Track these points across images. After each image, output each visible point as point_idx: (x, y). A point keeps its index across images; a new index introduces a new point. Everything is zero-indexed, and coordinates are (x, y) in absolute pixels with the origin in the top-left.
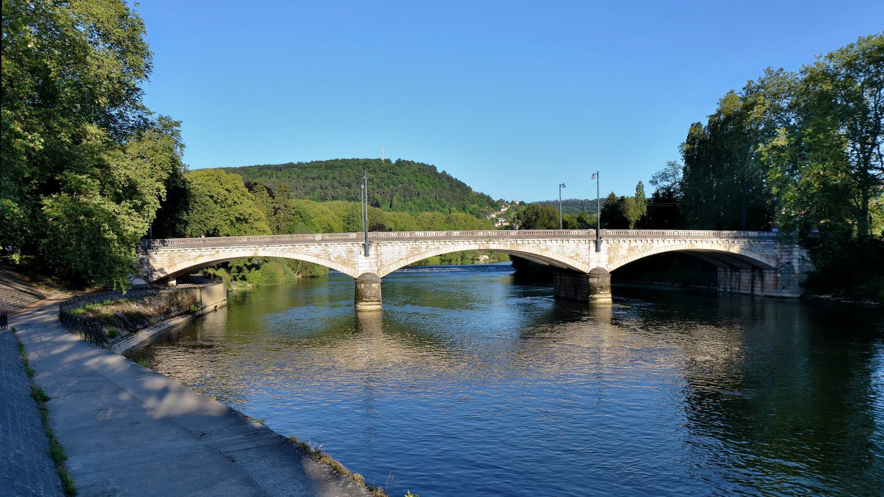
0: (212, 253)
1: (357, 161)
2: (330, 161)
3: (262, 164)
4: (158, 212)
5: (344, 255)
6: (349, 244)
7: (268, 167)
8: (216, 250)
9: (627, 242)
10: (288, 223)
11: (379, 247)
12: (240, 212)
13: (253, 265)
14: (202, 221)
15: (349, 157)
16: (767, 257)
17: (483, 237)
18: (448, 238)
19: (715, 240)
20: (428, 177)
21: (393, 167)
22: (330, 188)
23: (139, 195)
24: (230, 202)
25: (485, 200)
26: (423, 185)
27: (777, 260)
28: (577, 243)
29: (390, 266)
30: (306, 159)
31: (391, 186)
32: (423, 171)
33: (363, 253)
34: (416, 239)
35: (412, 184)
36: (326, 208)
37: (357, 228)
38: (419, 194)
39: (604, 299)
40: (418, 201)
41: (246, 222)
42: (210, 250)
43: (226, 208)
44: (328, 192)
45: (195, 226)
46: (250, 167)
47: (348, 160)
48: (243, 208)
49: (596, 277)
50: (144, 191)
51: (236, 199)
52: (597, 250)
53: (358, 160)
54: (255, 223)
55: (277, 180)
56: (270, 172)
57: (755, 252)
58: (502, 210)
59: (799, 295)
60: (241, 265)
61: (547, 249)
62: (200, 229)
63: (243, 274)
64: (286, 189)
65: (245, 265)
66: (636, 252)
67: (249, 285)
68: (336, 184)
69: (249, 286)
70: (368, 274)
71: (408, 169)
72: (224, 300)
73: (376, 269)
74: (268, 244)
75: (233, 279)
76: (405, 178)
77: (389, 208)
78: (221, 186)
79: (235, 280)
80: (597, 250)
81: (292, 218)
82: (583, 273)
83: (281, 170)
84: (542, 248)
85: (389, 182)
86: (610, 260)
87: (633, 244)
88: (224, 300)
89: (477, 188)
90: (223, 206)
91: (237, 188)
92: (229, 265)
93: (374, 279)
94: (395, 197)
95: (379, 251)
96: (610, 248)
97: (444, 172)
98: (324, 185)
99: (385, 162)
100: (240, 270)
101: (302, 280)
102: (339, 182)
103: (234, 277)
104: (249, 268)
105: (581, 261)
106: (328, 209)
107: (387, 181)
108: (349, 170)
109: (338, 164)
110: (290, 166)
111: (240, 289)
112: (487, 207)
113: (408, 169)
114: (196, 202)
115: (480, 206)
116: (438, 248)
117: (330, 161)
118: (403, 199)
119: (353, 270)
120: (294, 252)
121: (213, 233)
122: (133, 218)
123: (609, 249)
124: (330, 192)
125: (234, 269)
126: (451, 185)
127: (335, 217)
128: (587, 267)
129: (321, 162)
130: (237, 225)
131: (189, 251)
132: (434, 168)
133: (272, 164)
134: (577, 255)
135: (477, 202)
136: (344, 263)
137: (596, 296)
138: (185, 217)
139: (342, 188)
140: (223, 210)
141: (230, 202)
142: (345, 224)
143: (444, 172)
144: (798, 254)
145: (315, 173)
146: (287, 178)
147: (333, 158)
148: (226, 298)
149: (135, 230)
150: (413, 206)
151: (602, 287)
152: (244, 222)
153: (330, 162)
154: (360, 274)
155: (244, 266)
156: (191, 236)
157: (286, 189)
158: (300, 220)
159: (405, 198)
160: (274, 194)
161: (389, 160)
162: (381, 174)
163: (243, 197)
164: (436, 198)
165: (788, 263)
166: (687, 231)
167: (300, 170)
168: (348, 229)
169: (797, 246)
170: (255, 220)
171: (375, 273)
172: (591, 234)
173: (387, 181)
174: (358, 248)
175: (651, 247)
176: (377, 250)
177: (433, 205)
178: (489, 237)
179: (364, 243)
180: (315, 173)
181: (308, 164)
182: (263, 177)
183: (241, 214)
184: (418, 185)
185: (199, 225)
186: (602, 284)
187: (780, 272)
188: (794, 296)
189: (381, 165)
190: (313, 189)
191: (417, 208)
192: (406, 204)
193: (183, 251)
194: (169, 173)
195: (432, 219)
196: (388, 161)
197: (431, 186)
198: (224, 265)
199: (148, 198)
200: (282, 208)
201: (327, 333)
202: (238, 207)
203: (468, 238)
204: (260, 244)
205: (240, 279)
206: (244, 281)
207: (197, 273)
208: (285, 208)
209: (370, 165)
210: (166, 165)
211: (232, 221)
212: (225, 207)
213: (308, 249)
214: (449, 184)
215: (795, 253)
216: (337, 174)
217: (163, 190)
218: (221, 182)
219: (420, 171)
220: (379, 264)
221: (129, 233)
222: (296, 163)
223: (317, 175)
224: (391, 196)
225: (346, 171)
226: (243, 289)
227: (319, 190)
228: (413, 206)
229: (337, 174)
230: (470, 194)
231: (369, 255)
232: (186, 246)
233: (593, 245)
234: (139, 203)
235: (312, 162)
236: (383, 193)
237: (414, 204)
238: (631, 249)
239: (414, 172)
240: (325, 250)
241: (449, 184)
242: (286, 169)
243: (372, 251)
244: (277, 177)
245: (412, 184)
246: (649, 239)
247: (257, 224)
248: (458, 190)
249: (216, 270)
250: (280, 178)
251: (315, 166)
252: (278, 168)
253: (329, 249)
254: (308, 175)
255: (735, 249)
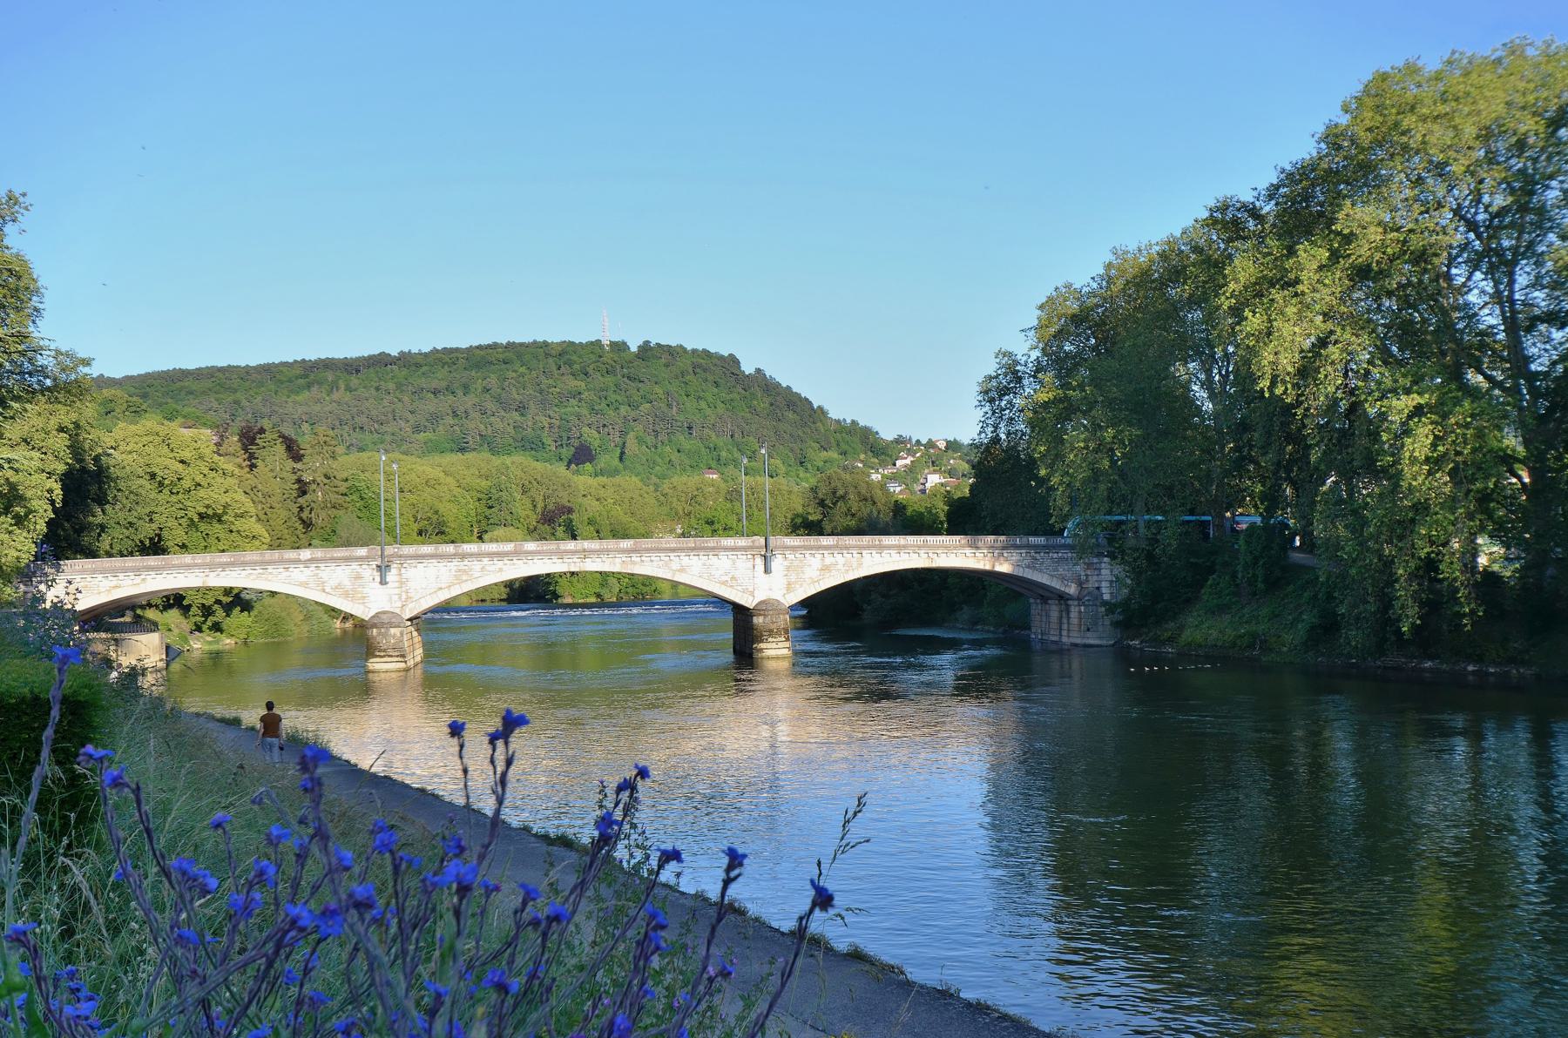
0: (135, 582)
1: (541, 349)
2: (477, 347)
3: (312, 356)
4: (50, 523)
5: (347, 583)
6: (355, 566)
7: (327, 364)
8: (142, 577)
9: (819, 556)
10: (333, 512)
11: (403, 571)
12: (207, 502)
13: (237, 601)
14: (130, 523)
15: (526, 338)
16: (1063, 579)
17: (574, 552)
18: (517, 553)
19: (968, 551)
20: (716, 384)
21: (631, 362)
22: (477, 415)
23: (21, 499)
24: (186, 483)
25: (856, 439)
26: (703, 404)
27: (1080, 584)
28: (733, 561)
29: (422, 601)
30: (421, 342)
31: (624, 410)
32: (705, 370)
33: (378, 579)
34: (463, 556)
35: (675, 404)
36: (436, 473)
37: (509, 518)
38: (690, 428)
39: (776, 650)
40: (687, 444)
41: (220, 521)
42: (133, 577)
43: (180, 496)
44: (472, 425)
45: (119, 533)
46: (282, 364)
47: (521, 345)
48: (212, 494)
49: (761, 615)
50: (29, 494)
51: (199, 478)
52: (767, 570)
53: (545, 344)
54: (236, 522)
55: (348, 397)
56: (330, 376)
57: (1041, 571)
58: (899, 463)
59: (1112, 642)
60: (209, 601)
61: (682, 570)
62: (128, 537)
63: (215, 619)
64: (328, 439)
65: (218, 602)
66: (833, 573)
67: (228, 641)
68: (490, 406)
69: (227, 642)
70: (385, 613)
71: (667, 366)
72: (161, 660)
73: (399, 604)
74: (224, 566)
75: (194, 628)
76: (658, 389)
77: (616, 462)
78: (171, 455)
79: (199, 629)
80: (767, 570)
81: (340, 501)
82: (748, 609)
83: (358, 371)
84: (674, 568)
85: (619, 398)
86: (789, 588)
87: (829, 560)
88: (161, 660)
89: (838, 411)
90: (174, 491)
91: (201, 458)
92: (185, 603)
93: (393, 620)
94: (631, 435)
95: (404, 576)
96: (789, 567)
97: (758, 371)
98: (462, 409)
99: (612, 350)
100: (207, 611)
101: (354, 632)
102: (498, 399)
103: (195, 624)
104: (228, 609)
105: (739, 588)
106: (442, 475)
107: (613, 397)
108: (523, 370)
109: (497, 356)
110: (380, 362)
111: (207, 648)
112: (862, 456)
113: (667, 366)
114: (119, 490)
115: (844, 453)
116: (501, 570)
117: (479, 347)
118: (650, 440)
119: (362, 607)
120: (266, 579)
121: (155, 547)
122: (15, 538)
123: (788, 568)
124: (475, 424)
125: (194, 610)
126: (772, 405)
127: (457, 491)
128: (751, 598)
129: (457, 350)
130: (203, 526)
131: (100, 579)
132: (733, 361)
133: (336, 357)
134: (733, 578)
135: (838, 445)
136: (346, 595)
137: (762, 645)
138: (99, 518)
139: (503, 413)
140: (174, 498)
141: (186, 483)
142: (482, 509)
143: (758, 371)
144: (1108, 572)
145: (440, 378)
146: (373, 391)
147: (486, 340)
148: (164, 657)
149: (18, 554)
150: (675, 457)
151: (771, 631)
152: (215, 521)
153: (478, 352)
154: (372, 613)
155: (215, 603)
156: (109, 555)
157: (328, 439)
158: (358, 505)
159: (656, 437)
160: (302, 452)
161: (624, 343)
162: (599, 380)
163: (213, 474)
164: (732, 436)
165: (1098, 588)
166: (922, 538)
167: (405, 372)
168: (489, 519)
169: (1106, 559)
170: (236, 516)
171: (398, 611)
172: (757, 544)
173: (613, 397)
174: (369, 572)
175: (860, 565)
176: (400, 575)
177: (724, 454)
178: (584, 551)
179: (379, 563)
180: (440, 378)
181: (426, 355)
182: (315, 389)
183: (208, 507)
184: (690, 404)
185: (125, 531)
186: (773, 627)
187: (1084, 604)
188: (1104, 642)
189: (600, 357)
190: (435, 418)
191: (687, 462)
192: (659, 450)
193: (89, 579)
194: (67, 464)
195: (696, 493)
196: (619, 347)
197: (721, 408)
198: (175, 600)
199: (35, 504)
200: (318, 480)
201: (867, 961)
202: (202, 493)
203: (550, 553)
204: (212, 567)
205: (210, 629)
206: (219, 633)
207: (123, 616)
208: (326, 481)
209: (574, 358)
210: (62, 453)
211: (191, 520)
212: (178, 492)
213: (288, 574)
214: (767, 400)
215: (1103, 572)
216: (493, 380)
217: (56, 492)
218: (171, 446)
219: (698, 370)
220: (404, 596)
221: (9, 558)
222: (394, 353)
223: (444, 384)
224: (623, 434)
225: (516, 371)
226: (215, 647)
227: (450, 420)
228: (675, 457)
229: (493, 380)
230: (819, 424)
231: (386, 583)
232: (94, 571)
233: (759, 562)
234: (22, 512)
235: (435, 351)
236: (604, 426)
237: (679, 451)
238: (826, 569)
239: (682, 373)
240: (317, 575)
241: (767, 400)
242: (371, 370)
243: (391, 576)
244: (348, 389)
245: (675, 404)
246: (855, 552)
247: (238, 524)
248: (790, 415)
249: (161, 611)
250: (355, 390)
251: (440, 360)
252: (352, 367)
253: (321, 574)
254: (423, 382)
255: (1004, 568)
